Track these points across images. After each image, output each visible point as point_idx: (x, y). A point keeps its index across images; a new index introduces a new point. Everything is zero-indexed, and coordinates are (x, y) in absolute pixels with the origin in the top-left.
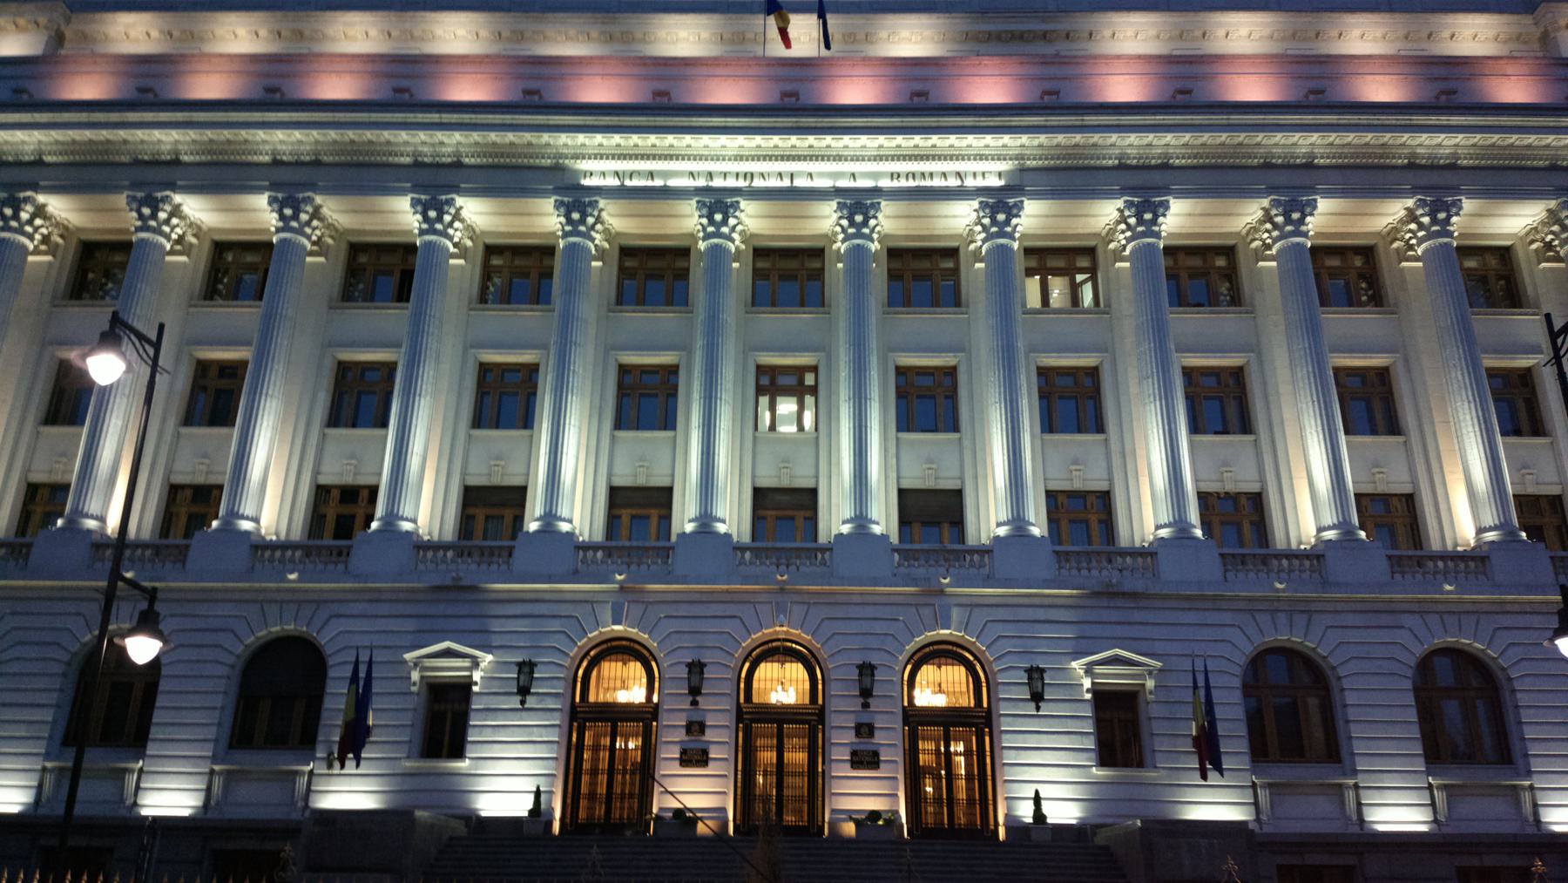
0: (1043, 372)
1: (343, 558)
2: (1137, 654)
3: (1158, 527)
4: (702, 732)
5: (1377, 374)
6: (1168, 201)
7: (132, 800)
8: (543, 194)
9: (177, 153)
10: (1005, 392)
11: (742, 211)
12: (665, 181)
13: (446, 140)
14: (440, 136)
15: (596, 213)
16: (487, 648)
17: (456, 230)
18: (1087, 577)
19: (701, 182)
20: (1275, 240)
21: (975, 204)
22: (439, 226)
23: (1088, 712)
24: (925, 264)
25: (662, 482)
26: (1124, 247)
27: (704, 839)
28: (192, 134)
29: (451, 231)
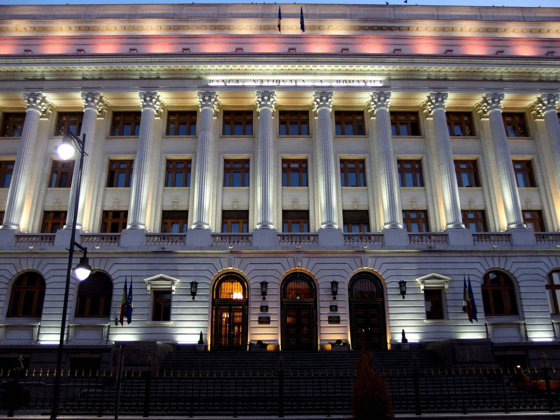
0: (400, 162)
1: (117, 240)
2: (442, 275)
3: (448, 224)
4: (267, 310)
5: (527, 163)
6: (447, 94)
7: (37, 339)
8: (193, 89)
9: (43, 75)
10: (387, 170)
11: (276, 96)
12: (243, 84)
13: (153, 69)
14: (151, 67)
15: (215, 97)
16: (177, 276)
17: (157, 105)
18: (421, 245)
19: (258, 84)
20: (488, 110)
21: (371, 93)
22: (151, 104)
23: (422, 298)
24: (349, 118)
25: (244, 208)
26: (430, 112)
27: (270, 352)
28: (50, 68)
29: (155, 106)
